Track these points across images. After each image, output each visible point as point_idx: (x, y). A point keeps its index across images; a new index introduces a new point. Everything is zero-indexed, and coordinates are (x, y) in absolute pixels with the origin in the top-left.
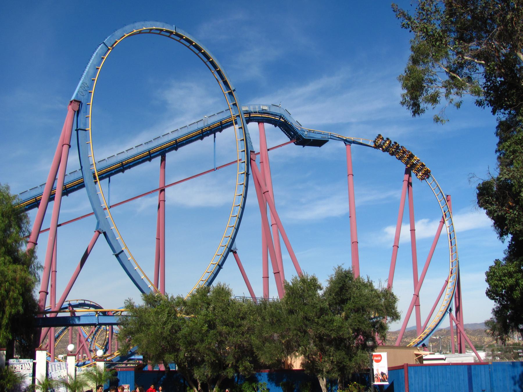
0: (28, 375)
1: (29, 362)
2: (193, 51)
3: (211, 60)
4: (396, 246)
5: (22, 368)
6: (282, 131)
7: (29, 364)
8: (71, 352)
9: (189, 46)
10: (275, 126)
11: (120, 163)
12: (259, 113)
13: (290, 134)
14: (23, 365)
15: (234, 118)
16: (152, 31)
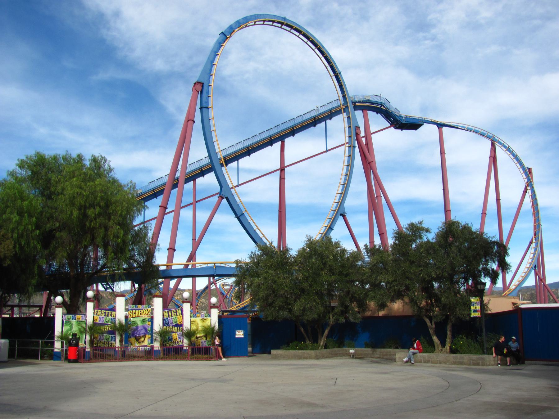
0: (147, 320)
1: (148, 308)
3: (311, 39)
4: (484, 214)
5: (141, 314)
6: (383, 117)
7: (147, 309)
8: (186, 299)
9: (290, 30)
10: (377, 114)
13: (390, 120)
14: (142, 310)
16: (257, 23)
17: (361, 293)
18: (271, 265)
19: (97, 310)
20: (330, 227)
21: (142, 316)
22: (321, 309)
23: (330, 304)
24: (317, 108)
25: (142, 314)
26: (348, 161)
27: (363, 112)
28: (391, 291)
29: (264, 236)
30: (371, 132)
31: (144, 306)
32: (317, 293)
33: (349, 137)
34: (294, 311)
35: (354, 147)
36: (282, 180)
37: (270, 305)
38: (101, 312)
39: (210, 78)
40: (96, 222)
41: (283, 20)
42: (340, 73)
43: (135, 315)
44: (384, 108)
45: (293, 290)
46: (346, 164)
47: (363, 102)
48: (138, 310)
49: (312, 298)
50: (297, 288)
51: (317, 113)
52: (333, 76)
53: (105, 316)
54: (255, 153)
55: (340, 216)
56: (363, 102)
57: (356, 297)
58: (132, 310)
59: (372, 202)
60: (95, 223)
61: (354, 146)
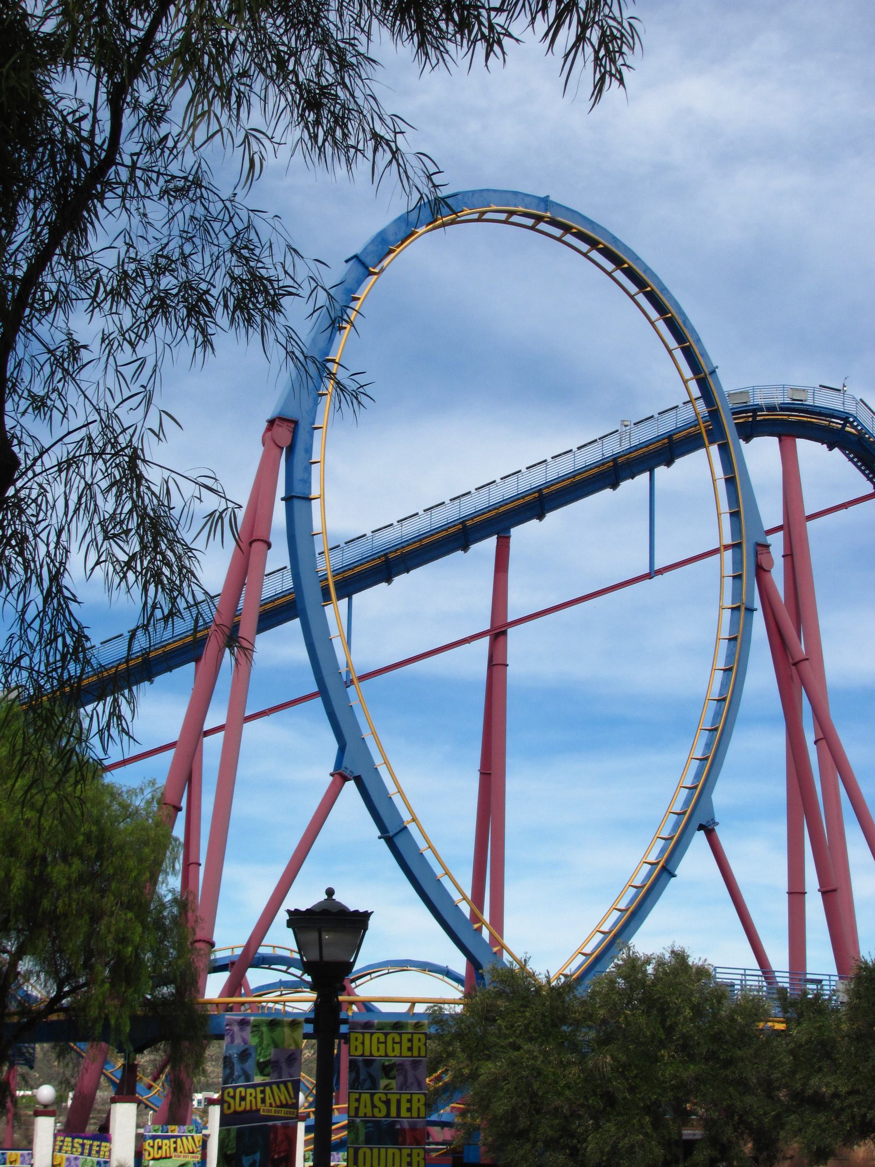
2: (721, 593)
3: (649, 289)
5: (175, 1149)
6: (851, 460)
7: (192, 1137)
10: (831, 448)
11: (379, 557)
12: (782, 409)
15: (705, 427)
17: (765, 1114)
18: (527, 1026)
19: (62, 1138)
20: (664, 869)
21: (179, 1156)
22: (659, 1152)
23: (680, 1134)
24: (626, 426)
25: (179, 1150)
26: (730, 656)
27: (780, 441)
28: (843, 1118)
29: (446, 874)
30: (807, 514)
31: (186, 1127)
32: (648, 1110)
33: (734, 577)
34: (584, 1155)
35: (750, 610)
36: (495, 669)
37: (522, 1135)
38: (72, 1142)
39: (316, 404)
40: (70, 898)
41: (542, 205)
42: (713, 372)
43: (243, 1103)
44: (853, 431)
45: (586, 1098)
46: (721, 664)
47: (782, 409)
48: (169, 1137)
49: (635, 1121)
50: (595, 1094)
51: (626, 446)
52: (691, 379)
53: (82, 1154)
54: (408, 572)
55: (699, 830)
56: (784, 408)
57: (751, 1122)
58: (154, 1138)
59: (800, 787)
60: (67, 902)
61: (749, 606)
